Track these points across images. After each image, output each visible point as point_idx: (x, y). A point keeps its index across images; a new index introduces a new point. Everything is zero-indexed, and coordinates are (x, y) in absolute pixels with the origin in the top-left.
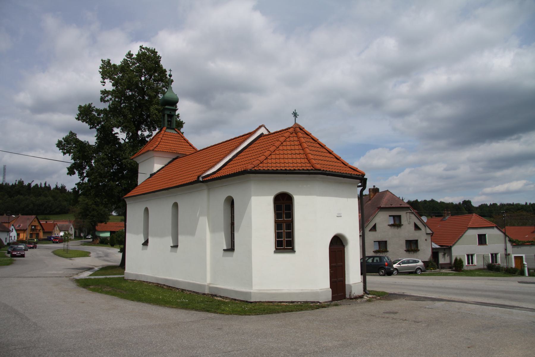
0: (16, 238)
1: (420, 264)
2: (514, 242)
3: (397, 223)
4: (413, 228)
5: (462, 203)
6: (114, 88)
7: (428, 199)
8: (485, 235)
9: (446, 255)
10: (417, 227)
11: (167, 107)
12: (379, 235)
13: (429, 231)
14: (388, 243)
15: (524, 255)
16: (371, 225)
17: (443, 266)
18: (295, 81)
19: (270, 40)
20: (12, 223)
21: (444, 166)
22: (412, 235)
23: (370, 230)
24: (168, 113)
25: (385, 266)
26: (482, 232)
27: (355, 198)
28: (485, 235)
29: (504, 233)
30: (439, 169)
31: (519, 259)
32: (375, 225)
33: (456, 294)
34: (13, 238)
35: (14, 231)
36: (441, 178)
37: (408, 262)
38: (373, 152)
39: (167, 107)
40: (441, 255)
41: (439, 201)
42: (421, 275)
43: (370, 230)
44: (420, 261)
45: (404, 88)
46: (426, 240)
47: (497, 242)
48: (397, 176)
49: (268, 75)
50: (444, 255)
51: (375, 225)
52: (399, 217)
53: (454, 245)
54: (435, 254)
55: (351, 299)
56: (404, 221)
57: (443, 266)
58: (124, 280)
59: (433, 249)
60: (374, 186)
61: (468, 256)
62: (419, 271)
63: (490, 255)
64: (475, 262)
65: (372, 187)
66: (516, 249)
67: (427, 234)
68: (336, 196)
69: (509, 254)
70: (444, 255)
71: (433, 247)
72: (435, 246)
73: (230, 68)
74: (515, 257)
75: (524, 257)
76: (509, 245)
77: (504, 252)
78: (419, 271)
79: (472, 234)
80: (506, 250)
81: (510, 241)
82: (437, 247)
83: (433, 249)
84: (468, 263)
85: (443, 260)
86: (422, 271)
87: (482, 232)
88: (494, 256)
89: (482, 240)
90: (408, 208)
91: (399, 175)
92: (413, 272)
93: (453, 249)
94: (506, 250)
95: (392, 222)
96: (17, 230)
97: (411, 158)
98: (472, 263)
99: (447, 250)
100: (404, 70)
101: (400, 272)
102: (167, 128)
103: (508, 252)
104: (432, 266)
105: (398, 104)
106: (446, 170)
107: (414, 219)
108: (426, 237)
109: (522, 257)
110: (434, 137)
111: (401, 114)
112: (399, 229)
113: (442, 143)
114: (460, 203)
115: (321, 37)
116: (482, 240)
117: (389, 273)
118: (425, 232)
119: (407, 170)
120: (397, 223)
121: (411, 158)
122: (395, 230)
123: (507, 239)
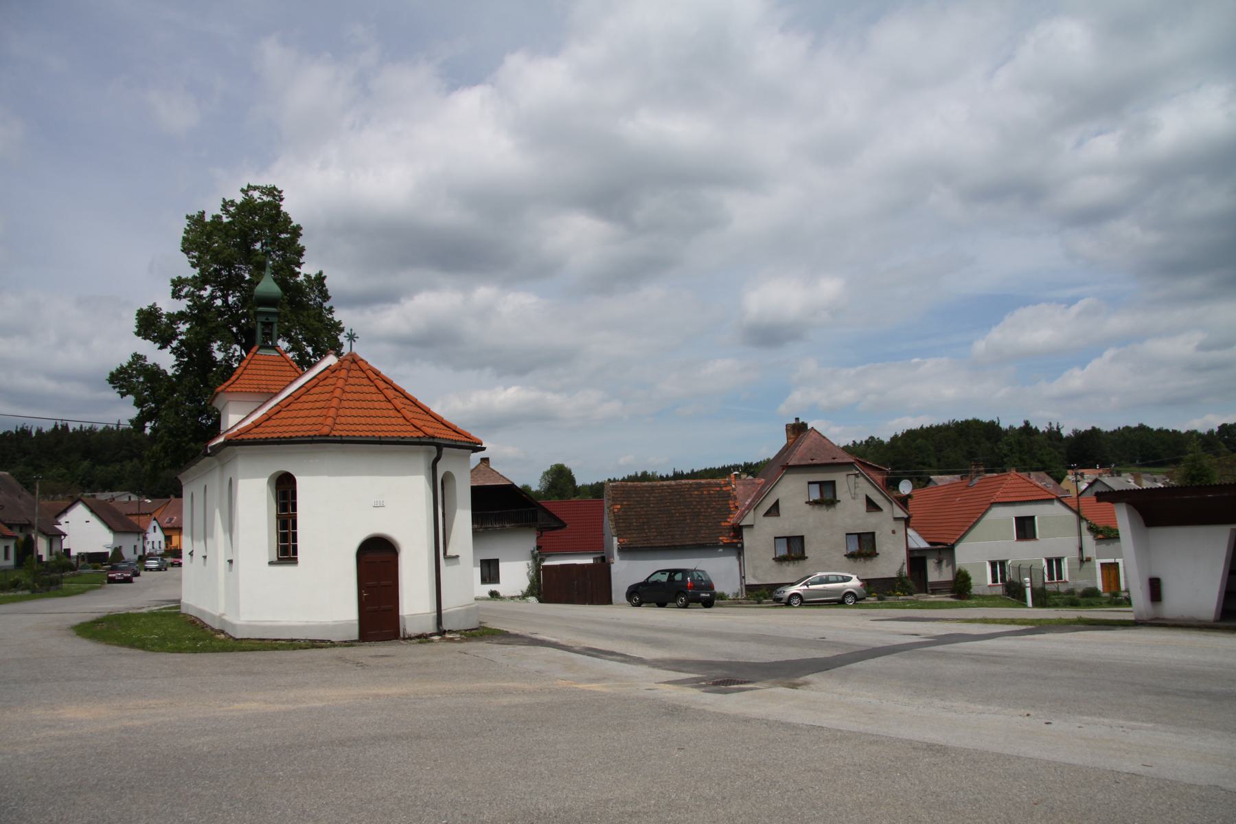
0: (163, 546)
1: (854, 583)
2: (1101, 532)
3: (827, 498)
4: (862, 506)
5: (1216, 430)
6: (196, 272)
7: (1134, 424)
8: (1033, 518)
9: (944, 563)
10: (872, 506)
11: (261, 309)
12: (785, 524)
13: (900, 513)
14: (806, 540)
15: (1119, 561)
16: (768, 503)
17: (937, 588)
18: (834, 152)
19: (774, 54)
20: (156, 515)
21: (1198, 337)
22: (868, 522)
23: (767, 514)
24: (263, 319)
25: (686, 587)
26: (1025, 511)
27: (415, 473)
28: (1033, 518)
29: (1078, 513)
30: (1183, 346)
31: (1111, 570)
32: (777, 503)
33: (607, 636)
34: (156, 546)
35: (158, 529)
36: (1193, 368)
37: (825, 580)
38: (1023, 313)
39: (261, 309)
40: (931, 564)
41: (1183, 431)
42: (855, 606)
43: (767, 514)
44: (854, 577)
45: (1105, 145)
46: (894, 532)
47: (1059, 534)
48: (1083, 368)
49: (768, 140)
50: (940, 562)
51: (777, 503)
52: (832, 484)
53: (958, 541)
54: (916, 561)
55: (404, 639)
56: (842, 492)
57: (937, 588)
58: (179, 613)
59: (910, 551)
60: (797, 419)
61: (993, 564)
62: (849, 600)
63: (1045, 563)
64: (1066, 575)
65: (793, 422)
66: (1103, 547)
67: (896, 519)
68: (412, 474)
69: (1089, 560)
70: (940, 562)
71: (913, 545)
72: (918, 542)
73: (679, 131)
74: (1102, 565)
75: (1121, 566)
76: (1088, 539)
77: (1076, 555)
78: (849, 600)
79: (1003, 517)
80: (1081, 549)
81: (1093, 530)
82: (923, 544)
83: (910, 551)
84: (1051, 577)
85: (935, 574)
86: (857, 599)
87: (1025, 511)
88: (1055, 563)
89: (1025, 529)
90: (851, 464)
91: (1088, 367)
92: (840, 601)
93: (957, 549)
94: (1081, 549)
95: (816, 496)
96: (163, 529)
97: (1117, 323)
98: (1060, 577)
99: (944, 551)
100: (1107, 101)
101: (803, 601)
102: (261, 347)
103: (1086, 555)
104: (911, 583)
105: (1093, 190)
106: (1202, 347)
107: (866, 488)
108: (893, 525)
109: (1102, 565)
110: (1172, 269)
111: (1093, 216)
112: (831, 510)
113: (1194, 284)
114: (1211, 432)
115: (897, 37)
116: (1025, 529)
117: (708, 604)
118: (890, 516)
119: (1109, 354)
120: (828, 496)
121: (1117, 323)
122: (822, 513)
123: (1084, 525)
